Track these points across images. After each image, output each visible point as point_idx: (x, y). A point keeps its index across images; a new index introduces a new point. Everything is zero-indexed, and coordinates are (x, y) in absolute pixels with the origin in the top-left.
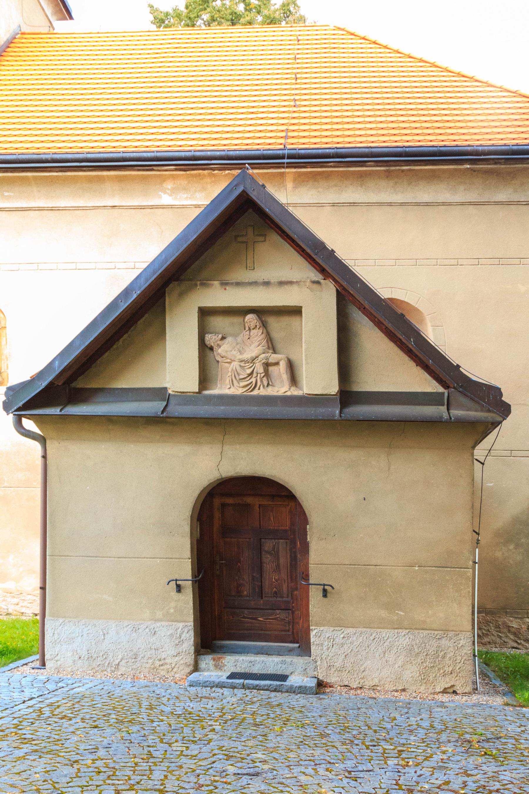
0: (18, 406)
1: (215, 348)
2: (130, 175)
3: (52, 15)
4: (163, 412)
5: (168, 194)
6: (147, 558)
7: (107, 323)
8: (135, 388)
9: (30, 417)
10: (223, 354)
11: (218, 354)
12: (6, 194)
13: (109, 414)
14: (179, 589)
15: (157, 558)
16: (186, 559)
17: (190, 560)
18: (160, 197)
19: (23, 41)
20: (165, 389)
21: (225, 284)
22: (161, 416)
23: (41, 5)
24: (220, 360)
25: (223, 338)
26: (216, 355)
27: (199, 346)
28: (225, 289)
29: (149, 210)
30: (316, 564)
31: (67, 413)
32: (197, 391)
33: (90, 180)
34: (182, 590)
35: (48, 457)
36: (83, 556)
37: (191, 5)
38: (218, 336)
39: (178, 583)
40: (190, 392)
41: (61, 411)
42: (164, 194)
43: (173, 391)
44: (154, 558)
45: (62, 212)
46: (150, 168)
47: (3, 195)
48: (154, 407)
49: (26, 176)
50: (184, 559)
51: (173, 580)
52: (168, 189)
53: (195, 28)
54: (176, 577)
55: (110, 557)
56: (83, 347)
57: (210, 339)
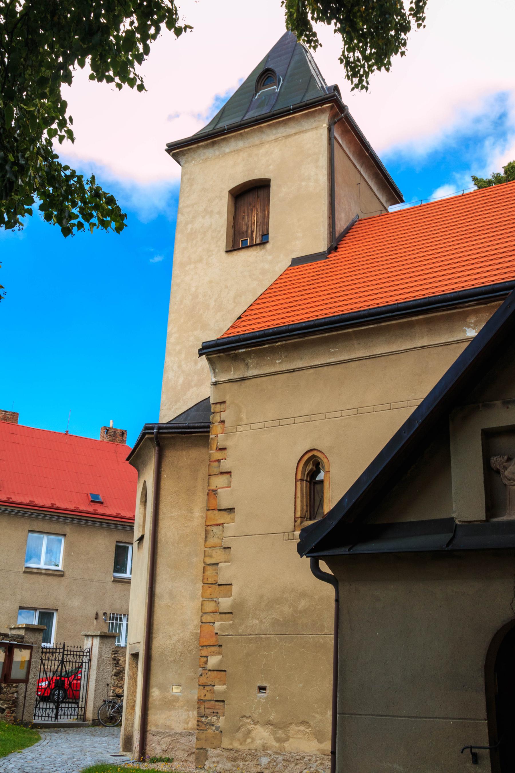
0: (310, 548)
1: (502, 470)
2: (436, 316)
3: (386, 202)
4: (448, 545)
5: (472, 327)
6: (439, 718)
7: (392, 455)
8: (423, 521)
9: (324, 558)
10: (510, 476)
11: (506, 477)
12: (332, 350)
13: (397, 551)
14: (476, 759)
15: (450, 718)
16: (482, 720)
17: (486, 722)
18: (465, 331)
19: (360, 226)
20: (453, 519)
21: (507, 403)
22: (446, 549)
23: (377, 196)
24: (507, 483)
25: (509, 459)
26: (503, 478)
27: (484, 469)
28: (508, 408)
29: (455, 345)
30: (460, 719)
31: (355, 552)
32: (485, 519)
33: (401, 326)
34: (479, 761)
35: (341, 601)
36: (372, 715)
37: (510, 171)
38: (503, 458)
39: (474, 750)
40: (477, 521)
41: (349, 550)
42: (468, 328)
43: (460, 521)
44: (447, 718)
45: (378, 359)
46: (454, 307)
47: (329, 352)
48: (438, 540)
49: (348, 332)
50: (480, 720)
51: (467, 748)
52: (472, 323)
53: (502, 184)
54: (472, 743)
55: (400, 717)
56: (370, 482)
57: (496, 461)
